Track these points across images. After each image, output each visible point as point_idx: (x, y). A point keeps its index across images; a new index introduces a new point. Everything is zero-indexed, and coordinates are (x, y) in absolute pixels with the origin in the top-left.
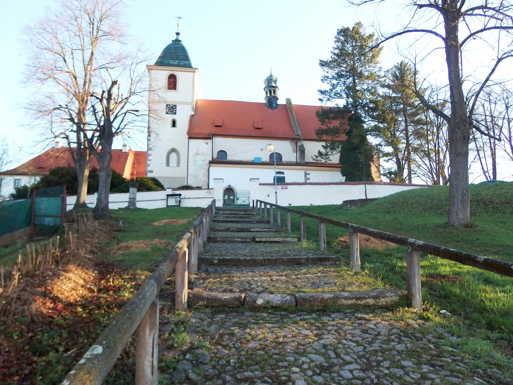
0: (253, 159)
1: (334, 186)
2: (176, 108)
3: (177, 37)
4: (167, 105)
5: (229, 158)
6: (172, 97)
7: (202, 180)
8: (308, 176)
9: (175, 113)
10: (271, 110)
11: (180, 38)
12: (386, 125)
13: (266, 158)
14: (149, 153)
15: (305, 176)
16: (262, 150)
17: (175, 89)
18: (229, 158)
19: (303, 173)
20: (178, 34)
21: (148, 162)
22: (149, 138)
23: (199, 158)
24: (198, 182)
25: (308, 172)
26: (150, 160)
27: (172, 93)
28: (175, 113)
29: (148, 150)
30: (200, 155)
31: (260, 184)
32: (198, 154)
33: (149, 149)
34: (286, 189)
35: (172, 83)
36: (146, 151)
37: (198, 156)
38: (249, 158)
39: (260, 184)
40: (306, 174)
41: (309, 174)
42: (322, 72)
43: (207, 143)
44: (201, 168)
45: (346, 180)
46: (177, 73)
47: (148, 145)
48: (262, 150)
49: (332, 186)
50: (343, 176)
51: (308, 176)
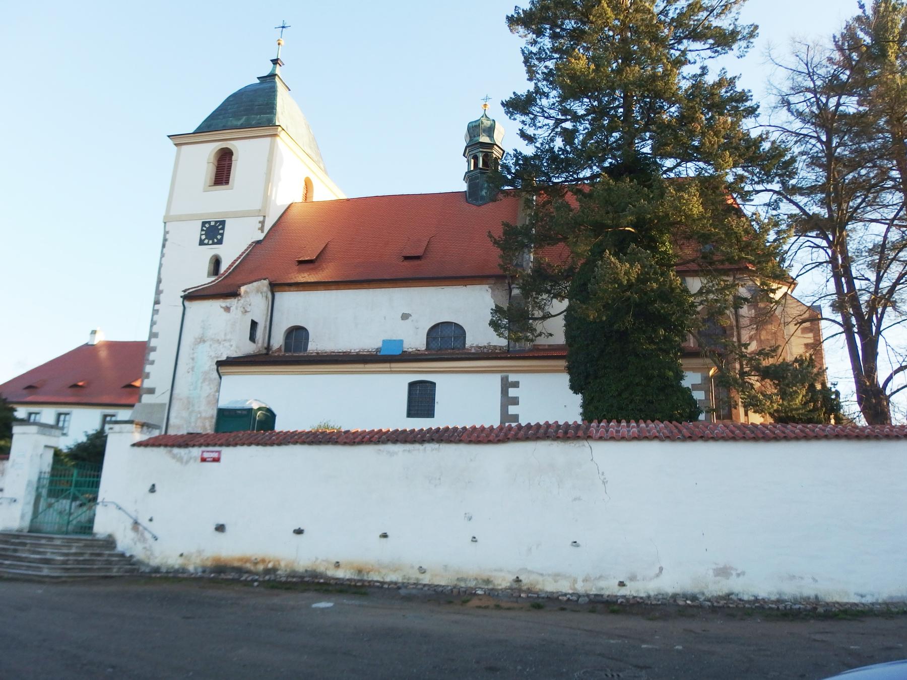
0: (379, 344)
1: (398, 448)
2: (223, 229)
3: (274, 69)
4: (204, 223)
5: (315, 345)
6: (218, 203)
7: (204, 415)
8: (512, 392)
9: (220, 242)
10: (474, 208)
11: (278, 70)
12: (612, 139)
13: (416, 341)
14: (154, 342)
15: (504, 392)
16: (405, 317)
17: (227, 183)
18: (315, 345)
19: (495, 381)
20: (275, 62)
21: (148, 368)
22: (157, 307)
23: (204, 348)
24: (193, 420)
25: (512, 378)
26: (152, 363)
27: (221, 192)
28: (220, 242)
29: (150, 338)
30: (207, 344)
31: (134, 445)
32: (202, 340)
33: (153, 335)
34: (216, 460)
35: (222, 171)
36: (146, 339)
37: (201, 346)
38: (369, 342)
39: (134, 445)
40: (506, 385)
41: (516, 385)
42: (520, 39)
43: (227, 309)
44: (204, 380)
45: (589, 412)
46: (233, 145)
47: (153, 323)
48: (405, 317)
49: (391, 447)
50: (576, 392)
51: (512, 392)
